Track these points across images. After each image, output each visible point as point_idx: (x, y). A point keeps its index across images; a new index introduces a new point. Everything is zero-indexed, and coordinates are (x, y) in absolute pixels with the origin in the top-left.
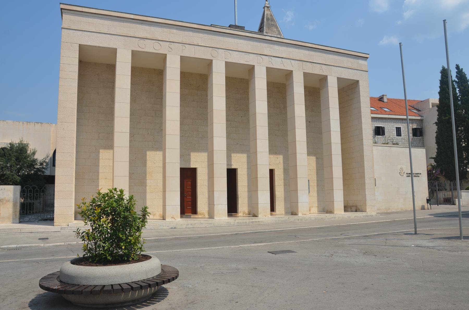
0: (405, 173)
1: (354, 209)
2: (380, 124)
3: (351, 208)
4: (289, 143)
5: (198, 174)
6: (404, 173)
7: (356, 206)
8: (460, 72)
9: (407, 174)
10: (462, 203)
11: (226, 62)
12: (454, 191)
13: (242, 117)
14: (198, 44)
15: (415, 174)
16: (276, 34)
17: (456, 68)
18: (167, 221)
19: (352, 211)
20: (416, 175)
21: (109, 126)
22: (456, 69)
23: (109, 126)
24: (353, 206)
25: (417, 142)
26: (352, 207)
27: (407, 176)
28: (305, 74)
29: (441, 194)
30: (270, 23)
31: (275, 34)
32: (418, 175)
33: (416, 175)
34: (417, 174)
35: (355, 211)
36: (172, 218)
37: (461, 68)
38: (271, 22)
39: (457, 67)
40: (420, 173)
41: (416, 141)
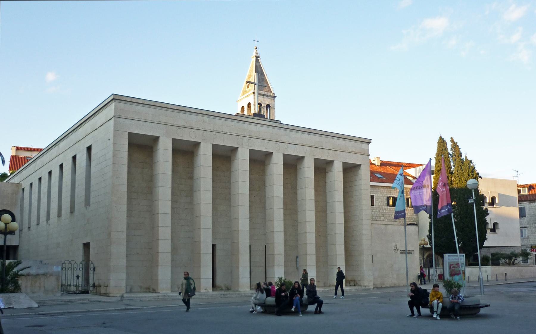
0: (399, 250)
1: (352, 284)
3: (350, 283)
5: (217, 250)
6: (398, 250)
7: (355, 281)
8: (455, 146)
9: (401, 251)
10: (481, 290)
11: (249, 149)
12: (430, 268)
13: (255, 197)
14: (227, 132)
15: (408, 251)
16: (266, 91)
17: (451, 142)
18: (317, 276)
19: (350, 285)
20: (409, 252)
21: (141, 204)
22: (451, 143)
23: (141, 204)
24: (351, 281)
25: (411, 213)
26: (350, 282)
27: (401, 253)
28: (315, 159)
29: (440, 272)
30: (260, 77)
31: (265, 90)
32: (410, 252)
33: (409, 252)
34: (410, 251)
35: (353, 285)
36: (205, 289)
37: (455, 142)
38: (261, 76)
39: (452, 140)
40: (413, 250)
41: (410, 212)
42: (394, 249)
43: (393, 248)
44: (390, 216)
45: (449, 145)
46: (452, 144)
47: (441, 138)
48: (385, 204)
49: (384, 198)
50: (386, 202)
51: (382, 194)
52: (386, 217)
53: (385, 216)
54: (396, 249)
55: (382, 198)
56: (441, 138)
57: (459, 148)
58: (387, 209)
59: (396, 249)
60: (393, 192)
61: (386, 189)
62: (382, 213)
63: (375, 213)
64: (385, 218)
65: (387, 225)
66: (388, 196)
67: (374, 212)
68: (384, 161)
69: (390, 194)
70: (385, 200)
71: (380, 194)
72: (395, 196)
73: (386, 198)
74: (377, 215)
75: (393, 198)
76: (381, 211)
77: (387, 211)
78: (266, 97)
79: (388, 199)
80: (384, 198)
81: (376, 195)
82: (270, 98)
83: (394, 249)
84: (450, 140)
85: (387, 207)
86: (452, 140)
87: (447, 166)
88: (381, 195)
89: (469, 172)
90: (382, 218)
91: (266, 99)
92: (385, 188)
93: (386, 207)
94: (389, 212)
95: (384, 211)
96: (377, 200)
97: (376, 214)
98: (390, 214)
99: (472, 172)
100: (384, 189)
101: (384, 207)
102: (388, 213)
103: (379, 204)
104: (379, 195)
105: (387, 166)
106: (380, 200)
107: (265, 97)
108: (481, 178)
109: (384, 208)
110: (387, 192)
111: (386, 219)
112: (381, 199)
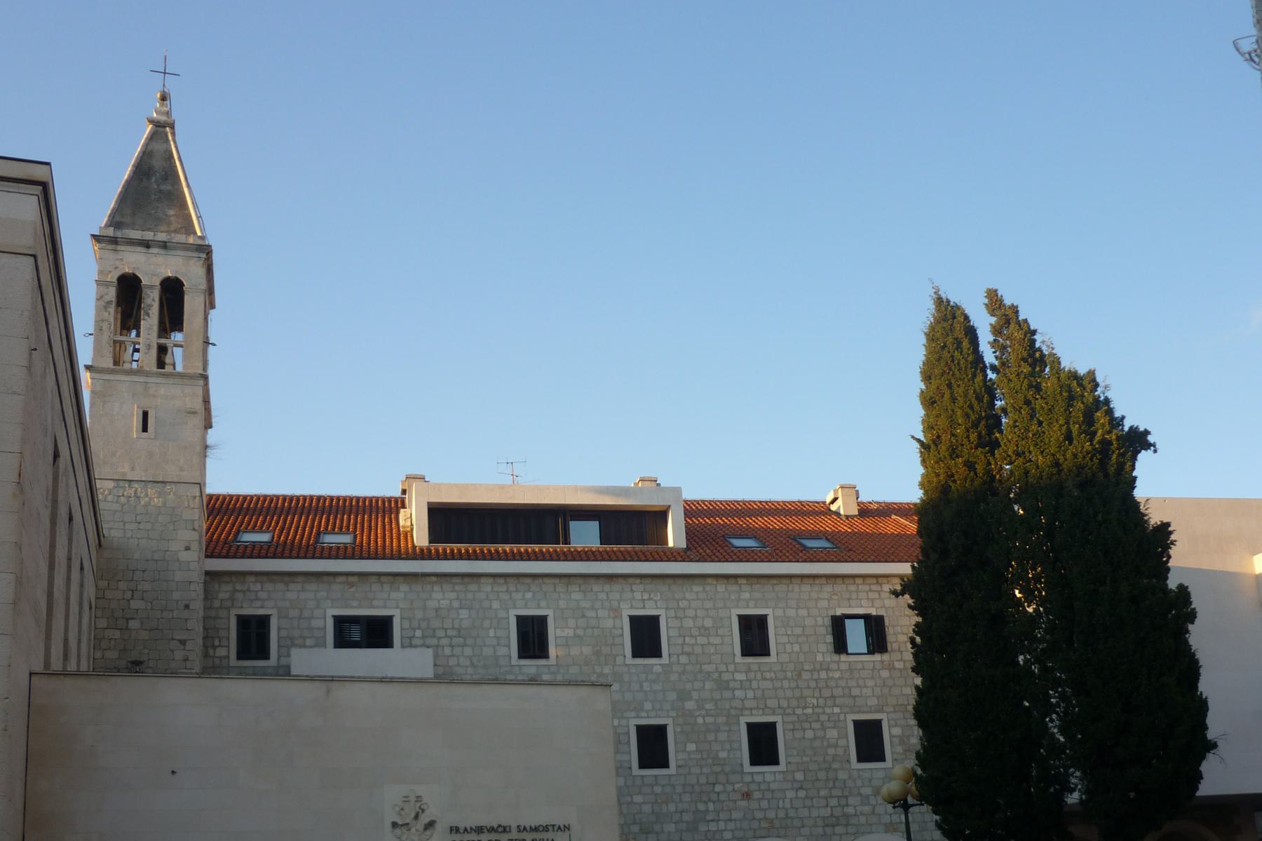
2: (539, 607)
4: (196, 540)
34: (536, 829)
39: (995, 302)
42: (394, 825)
43: (391, 817)
44: (855, 692)
45: (983, 323)
46: (993, 320)
47: (940, 302)
48: (823, 648)
49: (820, 620)
50: (830, 639)
51: (808, 609)
52: (833, 697)
53: (827, 693)
54: (409, 819)
55: (808, 622)
56: (940, 302)
57: (1032, 328)
58: (834, 666)
59: (409, 819)
60: (862, 595)
61: (828, 588)
62: (813, 684)
63: (778, 684)
64: (829, 702)
65: (334, 685)
66: (838, 613)
67: (771, 679)
68: (895, 504)
69: (850, 606)
70: (822, 631)
71: (798, 608)
72: (873, 612)
73: (828, 622)
74: (789, 693)
75: (866, 618)
76: (806, 676)
77: (837, 675)
78: (162, 251)
79: (838, 624)
80: (820, 620)
81: (779, 612)
82: (179, 252)
83: (394, 825)
84: (986, 305)
85: (836, 657)
86: (995, 302)
87: (968, 416)
88: (803, 612)
89: (1067, 423)
90: (815, 701)
91: (160, 260)
92: (823, 581)
93: (828, 659)
94: (847, 675)
95: (824, 672)
96: (782, 631)
97: (782, 687)
98: (852, 683)
99: (1089, 419)
100: (816, 588)
101: (820, 658)
102: (842, 683)
103: (796, 648)
104: (791, 613)
105: (894, 517)
106: (798, 631)
107: (154, 250)
108: (1155, 451)
109: (821, 664)
110: (829, 600)
111: (835, 706)
112: (804, 627)
